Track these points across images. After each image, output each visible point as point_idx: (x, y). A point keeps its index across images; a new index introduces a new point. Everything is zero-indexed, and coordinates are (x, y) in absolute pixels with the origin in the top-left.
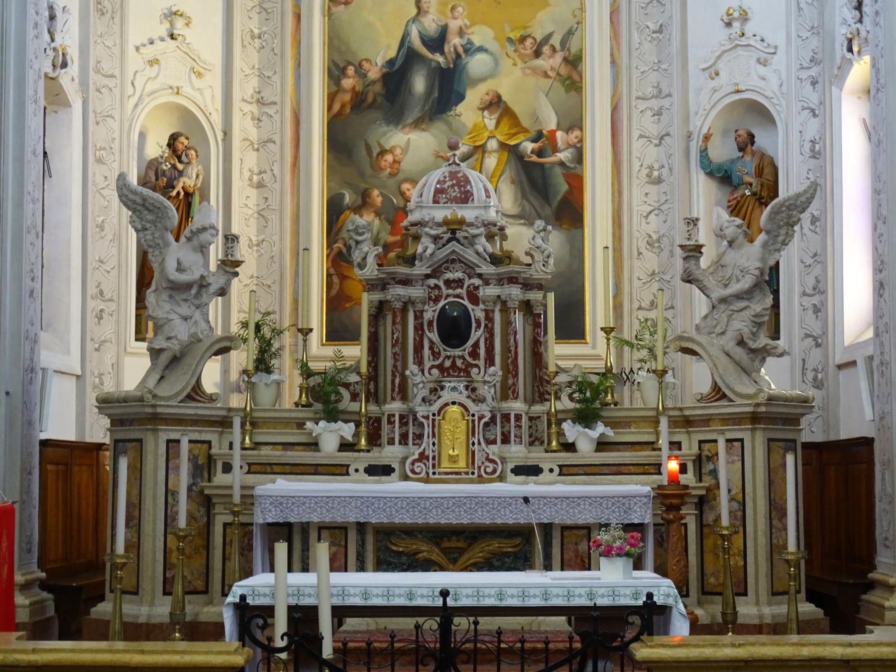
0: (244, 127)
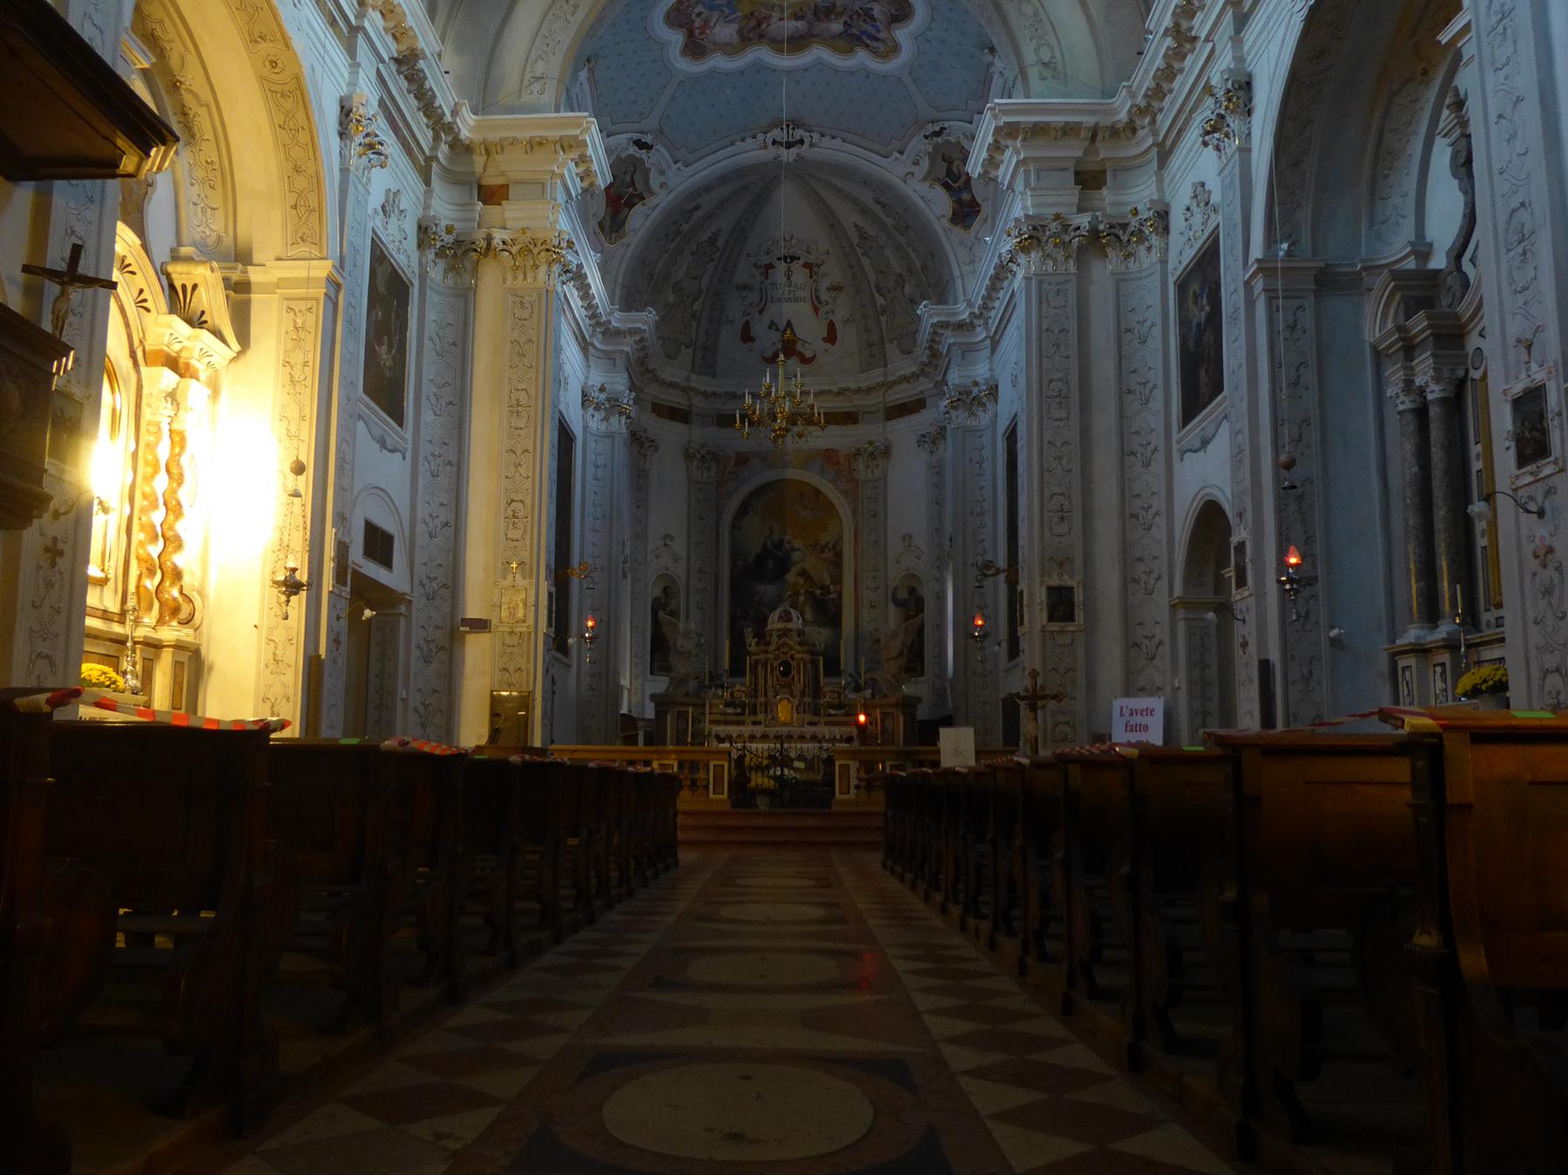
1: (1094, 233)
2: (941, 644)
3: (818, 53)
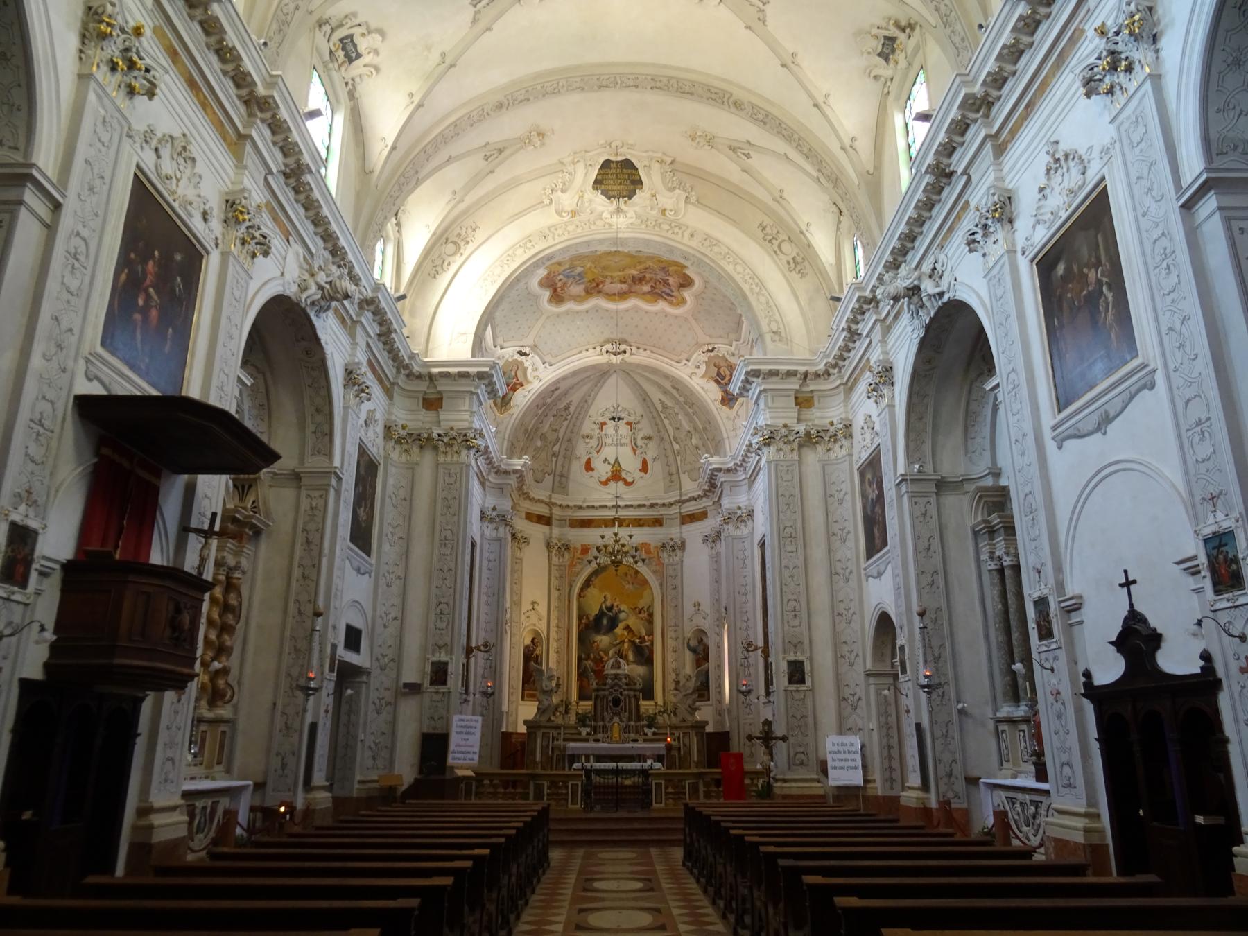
0: (553, 635)
1: (808, 434)
2: (720, 678)
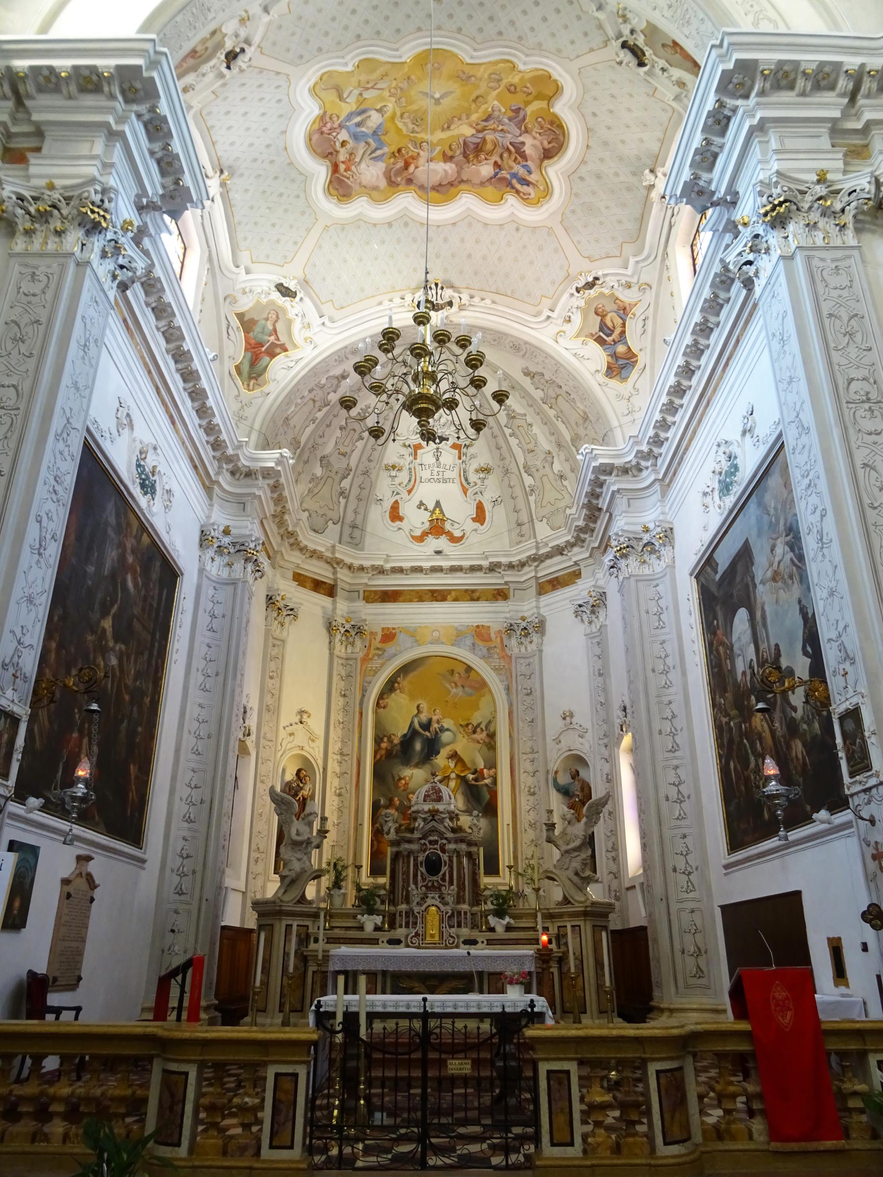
3: (466, 203)
